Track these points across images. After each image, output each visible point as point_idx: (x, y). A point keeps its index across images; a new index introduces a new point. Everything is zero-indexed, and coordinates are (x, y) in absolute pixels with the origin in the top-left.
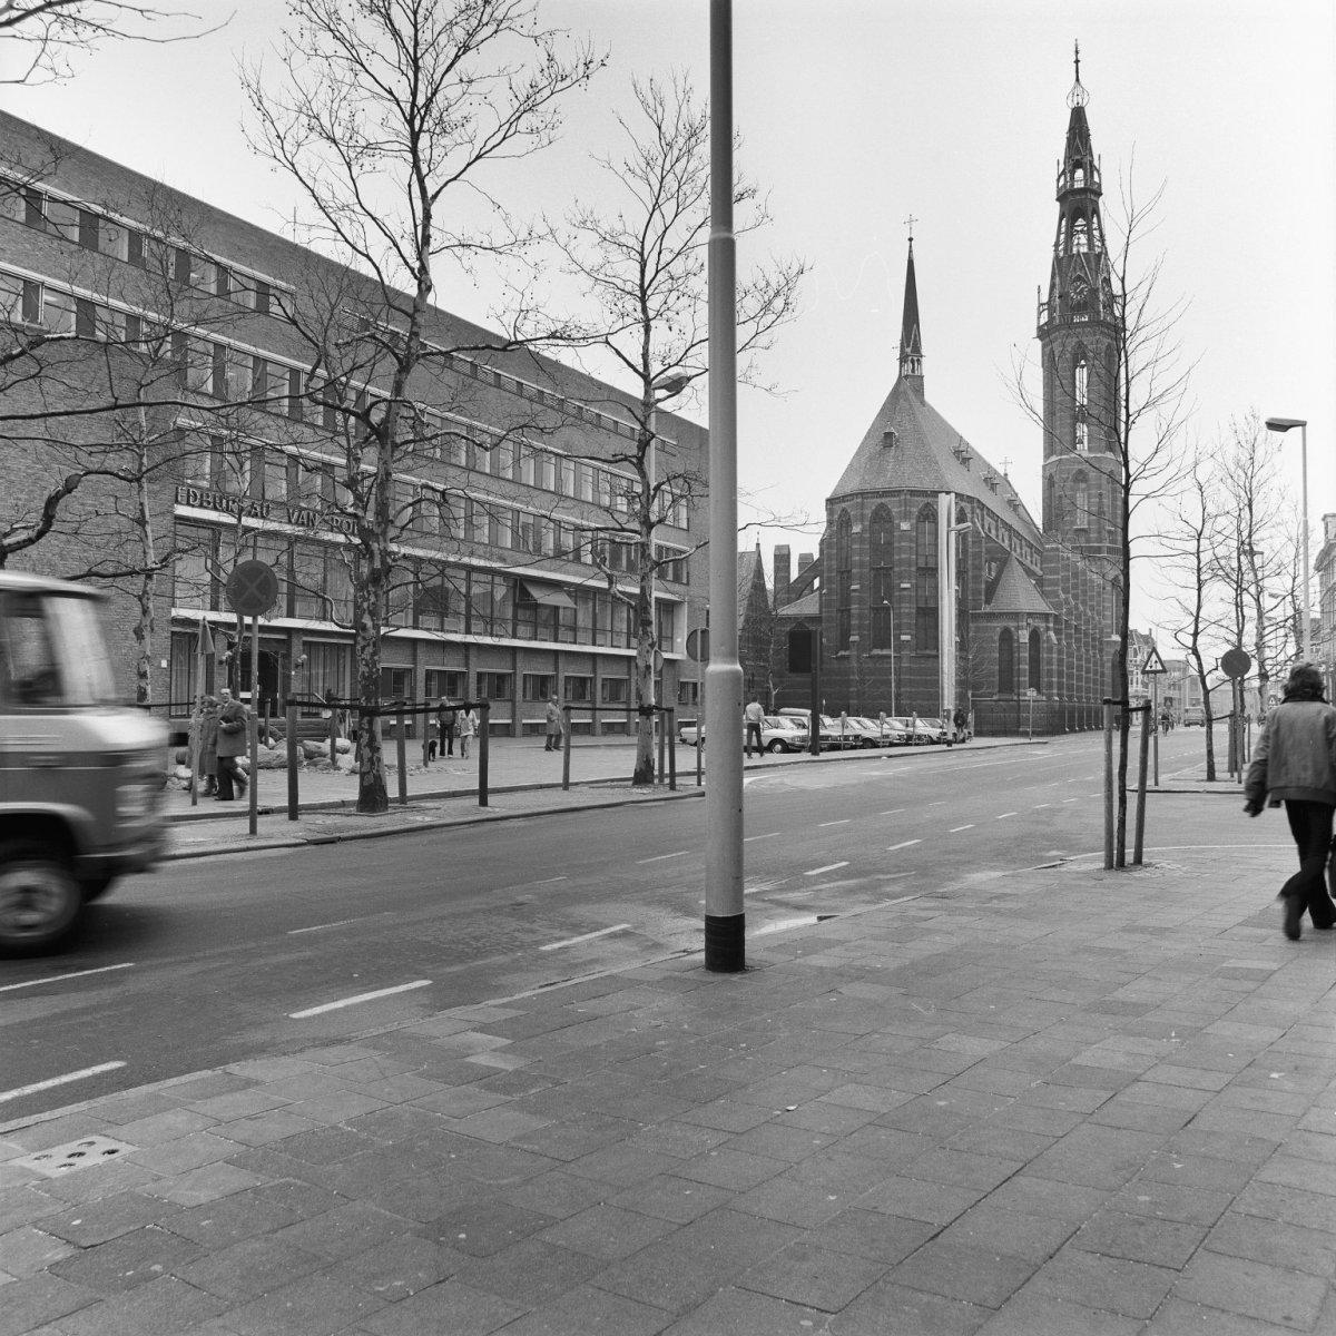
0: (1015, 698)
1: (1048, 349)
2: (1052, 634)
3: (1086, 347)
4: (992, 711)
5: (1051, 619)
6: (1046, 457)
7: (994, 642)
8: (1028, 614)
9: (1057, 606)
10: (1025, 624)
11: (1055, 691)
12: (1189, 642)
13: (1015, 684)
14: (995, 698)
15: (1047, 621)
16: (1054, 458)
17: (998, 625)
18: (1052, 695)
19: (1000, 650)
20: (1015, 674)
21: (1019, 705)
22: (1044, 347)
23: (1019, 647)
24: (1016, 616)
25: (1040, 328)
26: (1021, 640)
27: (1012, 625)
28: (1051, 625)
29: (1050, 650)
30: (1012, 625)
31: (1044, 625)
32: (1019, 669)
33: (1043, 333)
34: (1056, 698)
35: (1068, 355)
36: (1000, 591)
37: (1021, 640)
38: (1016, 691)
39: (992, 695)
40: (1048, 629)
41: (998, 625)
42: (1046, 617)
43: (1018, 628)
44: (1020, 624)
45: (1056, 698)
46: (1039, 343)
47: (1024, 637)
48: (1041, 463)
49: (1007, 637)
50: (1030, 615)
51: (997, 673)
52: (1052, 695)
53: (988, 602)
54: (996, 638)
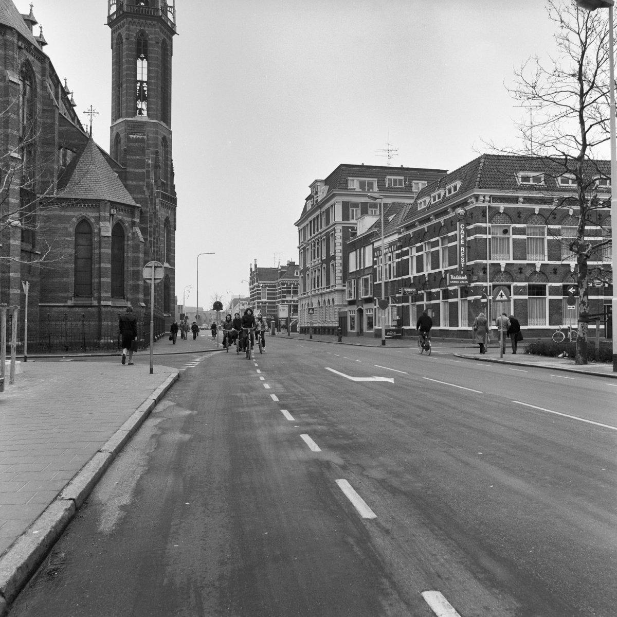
0: (95, 303)
1: (116, 35)
2: (138, 230)
3: (147, 36)
4: (66, 318)
5: (137, 213)
6: (113, 120)
7: (69, 235)
8: (112, 203)
9: (144, 201)
10: (107, 214)
11: (141, 296)
12: (605, 131)
13: (95, 286)
14: (70, 303)
15: (133, 216)
16: (121, 120)
17: (75, 215)
18: (138, 300)
19: (76, 245)
20: (95, 273)
21: (100, 312)
22: (113, 32)
23: (100, 242)
24: (96, 204)
25: (109, 17)
26: (103, 234)
27: (91, 215)
28: (137, 220)
29: (136, 248)
30: (91, 215)
31: (129, 219)
32: (100, 268)
33: (111, 23)
34: (143, 304)
35: (133, 39)
36: (76, 176)
37: (103, 234)
38: (96, 295)
39: (65, 299)
40: (133, 224)
41: (75, 215)
42: (130, 210)
43: (99, 219)
44: (102, 214)
45: (143, 304)
46: (109, 30)
47: (107, 229)
48: (110, 125)
49: (85, 228)
50: (114, 204)
51: (72, 272)
52: (138, 300)
53: (61, 185)
54: (71, 230)
